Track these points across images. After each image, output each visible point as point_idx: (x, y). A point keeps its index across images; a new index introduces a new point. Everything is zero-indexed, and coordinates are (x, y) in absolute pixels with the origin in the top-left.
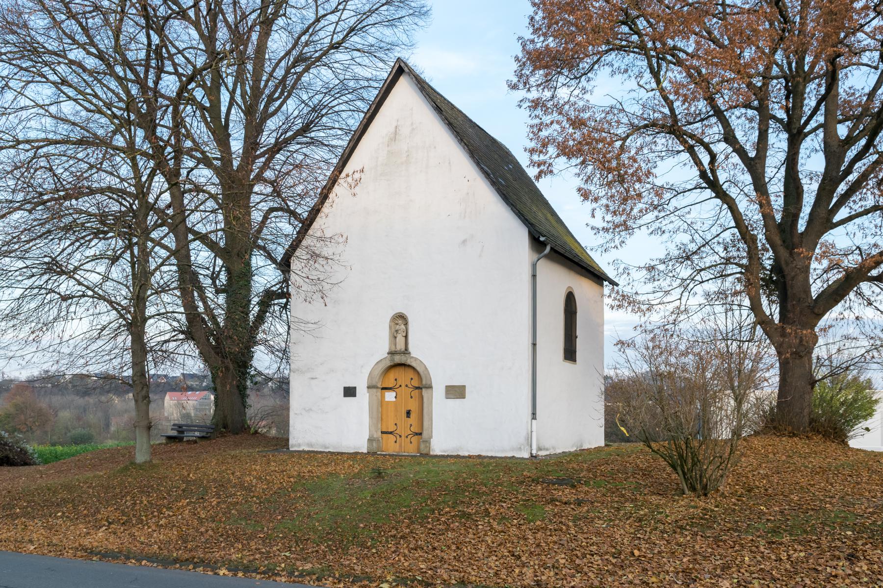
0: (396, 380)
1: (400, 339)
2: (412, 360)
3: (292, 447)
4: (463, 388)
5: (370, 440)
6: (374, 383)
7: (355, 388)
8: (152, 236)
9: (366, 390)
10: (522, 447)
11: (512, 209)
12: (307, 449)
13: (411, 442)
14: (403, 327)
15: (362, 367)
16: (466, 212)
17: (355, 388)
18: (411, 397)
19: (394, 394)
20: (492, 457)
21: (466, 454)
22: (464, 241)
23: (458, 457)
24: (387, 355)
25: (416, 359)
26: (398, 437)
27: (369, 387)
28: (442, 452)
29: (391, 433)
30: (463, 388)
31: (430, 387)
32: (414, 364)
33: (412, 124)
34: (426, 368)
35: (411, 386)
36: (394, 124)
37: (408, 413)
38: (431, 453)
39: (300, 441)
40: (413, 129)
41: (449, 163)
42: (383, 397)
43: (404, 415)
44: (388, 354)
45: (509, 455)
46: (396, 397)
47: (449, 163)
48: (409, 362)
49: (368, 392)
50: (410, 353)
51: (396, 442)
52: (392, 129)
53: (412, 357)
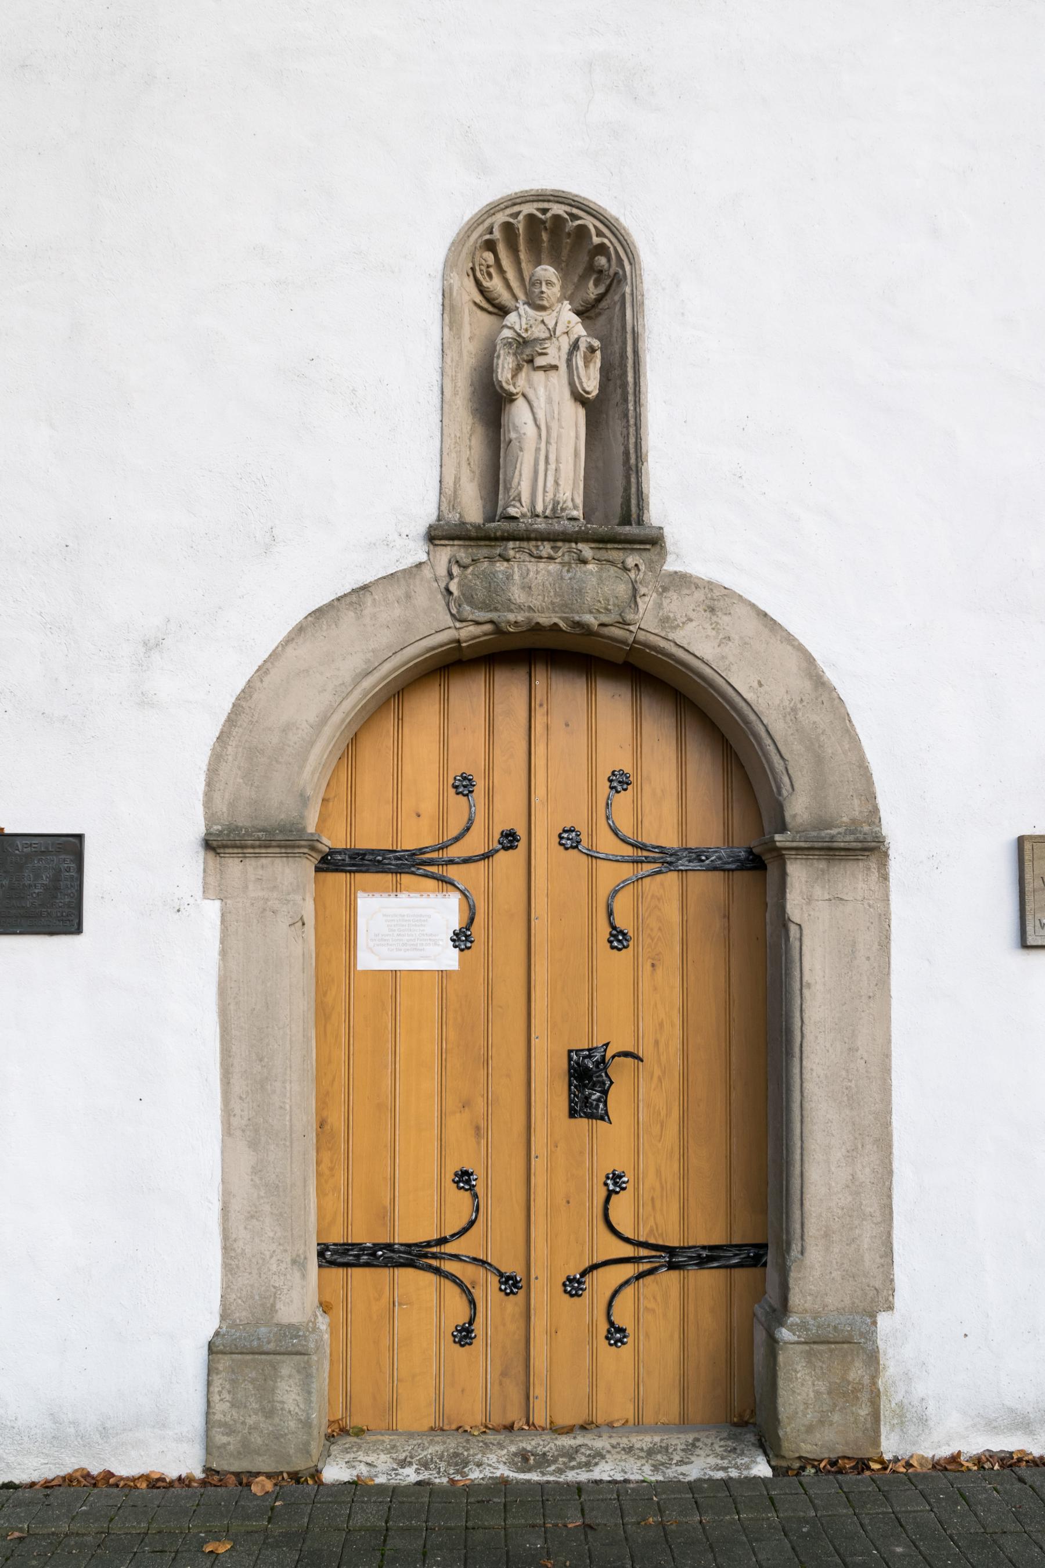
0: (464, 785)
2: (675, 605)
8: (756, 1305)
11: (675, 656)
13: (616, 1334)
15: (151, 646)
18: (618, 938)
24: (418, 552)
26: (487, 1289)
27: (212, 845)
28: (992, 1427)
34: (819, 682)
35: (607, 844)
38: (890, 1446)
44: (435, 536)
46: (462, 939)
50: (654, 542)
51: (464, 1335)
53: (682, 581)
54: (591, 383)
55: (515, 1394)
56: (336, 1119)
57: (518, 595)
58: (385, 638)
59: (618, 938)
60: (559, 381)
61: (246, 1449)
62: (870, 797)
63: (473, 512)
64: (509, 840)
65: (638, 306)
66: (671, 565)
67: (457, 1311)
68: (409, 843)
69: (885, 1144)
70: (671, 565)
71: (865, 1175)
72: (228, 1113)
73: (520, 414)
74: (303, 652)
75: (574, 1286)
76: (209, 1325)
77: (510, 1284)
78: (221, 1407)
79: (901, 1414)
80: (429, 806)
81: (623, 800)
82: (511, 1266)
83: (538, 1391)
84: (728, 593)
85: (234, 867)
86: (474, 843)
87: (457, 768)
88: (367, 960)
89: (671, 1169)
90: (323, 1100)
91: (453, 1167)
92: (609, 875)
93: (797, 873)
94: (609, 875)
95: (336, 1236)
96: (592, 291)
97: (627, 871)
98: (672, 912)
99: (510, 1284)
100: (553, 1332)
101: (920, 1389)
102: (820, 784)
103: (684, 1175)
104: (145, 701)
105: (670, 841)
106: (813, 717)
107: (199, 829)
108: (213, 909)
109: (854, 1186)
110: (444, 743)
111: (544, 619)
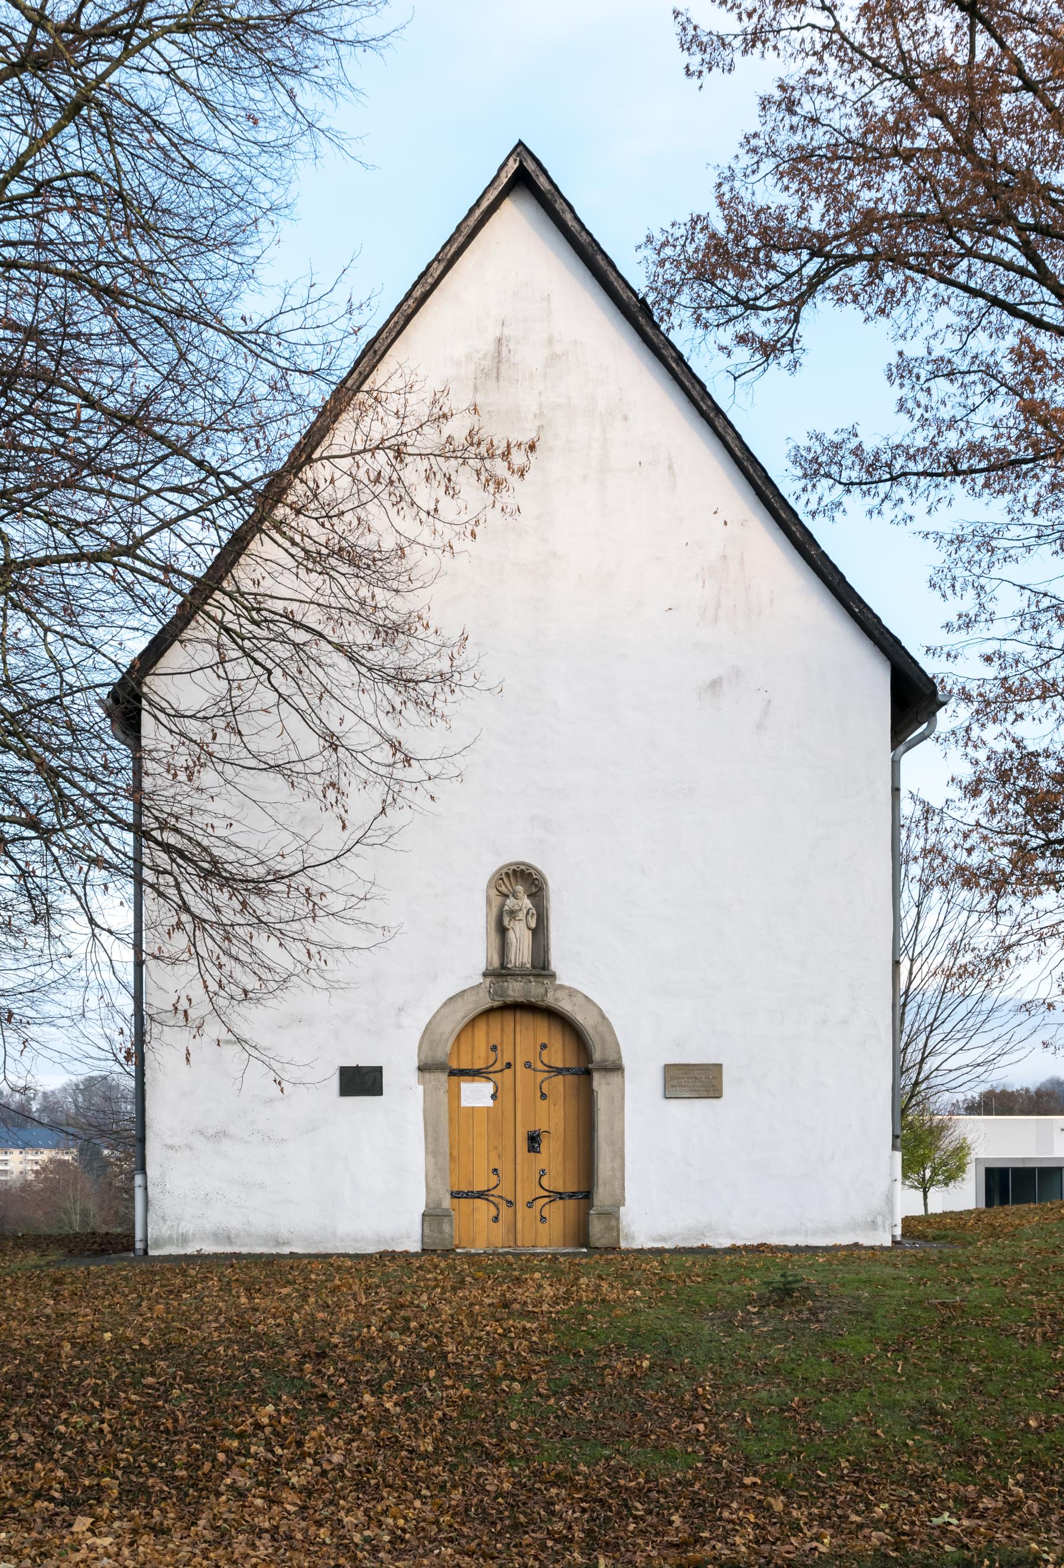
0: (494, 1048)
1: (520, 937)
2: (560, 994)
3: (158, 1244)
4: (716, 1069)
5: (432, 1216)
6: (440, 1055)
7: (379, 1070)
9: (413, 1075)
10: (879, 1220)
12: (209, 1248)
13: (543, 1219)
14: (527, 903)
15: (401, 1009)
16: (718, 607)
17: (379, 1070)
18: (543, 1096)
19: (488, 1088)
20: (797, 1249)
21: (726, 1243)
22: (715, 684)
23: (706, 1251)
25: (572, 992)
26: (503, 1205)
27: (420, 1069)
28: (654, 1240)
29: (481, 1195)
30: (716, 1069)
31: (617, 1068)
32: (566, 1006)
33: (550, 341)
34: (604, 1017)
35: (540, 1066)
36: (494, 332)
37: (534, 1141)
38: (623, 1245)
39: (187, 1227)
40: (555, 356)
41: (670, 467)
42: (455, 1096)
43: (522, 1144)
44: (485, 975)
45: (846, 1239)
46: (494, 1097)
47: (670, 467)
48: (550, 1000)
49: (421, 1082)
50: (553, 976)
51: (496, 1219)
52: (487, 345)
53: (562, 987)
54: (533, 925)
55: (512, 1238)
56: (455, 1153)
57: (511, 993)
58: (471, 1006)
59: (543, 1096)
60: (523, 924)
61: (434, 1243)
62: (619, 1052)
63: (496, 963)
64: (509, 1065)
65: (548, 900)
66: (558, 982)
67: (493, 1212)
68: (477, 1067)
69: (622, 1157)
70: (558, 982)
71: (616, 1166)
72: (427, 1147)
73: (511, 935)
74: (446, 1011)
75: (530, 1205)
76: (422, 1209)
77: (510, 1203)
78: (427, 1231)
79: (627, 1236)
80: (483, 1055)
81: (545, 1052)
82: (510, 1198)
83: (519, 1236)
84: (576, 991)
85: (427, 1075)
86: (498, 1066)
87: (492, 1043)
88: (464, 1103)
89: (560, 1168)
90: (451, 1147)
91: (492, 1168)
92: (541, 1076)
93: (596, 1076)
94: (541, 1076)
95: (456, 1189)
96: (534, 890)
97: (546, 1075)
98: (561, 1088)
99: (510, 1203)
100: (524, 1219)
101: (632, 1229)
102: (604, 1049)
103: (564, 1170)
104: (399, 1026)
105: (560, 1065)
106: (602, 1028)
107: (416, 1064)
108: (421, 1088)
109: (613, 1169)
110: (488, 1035)
111: (519, 1000)
